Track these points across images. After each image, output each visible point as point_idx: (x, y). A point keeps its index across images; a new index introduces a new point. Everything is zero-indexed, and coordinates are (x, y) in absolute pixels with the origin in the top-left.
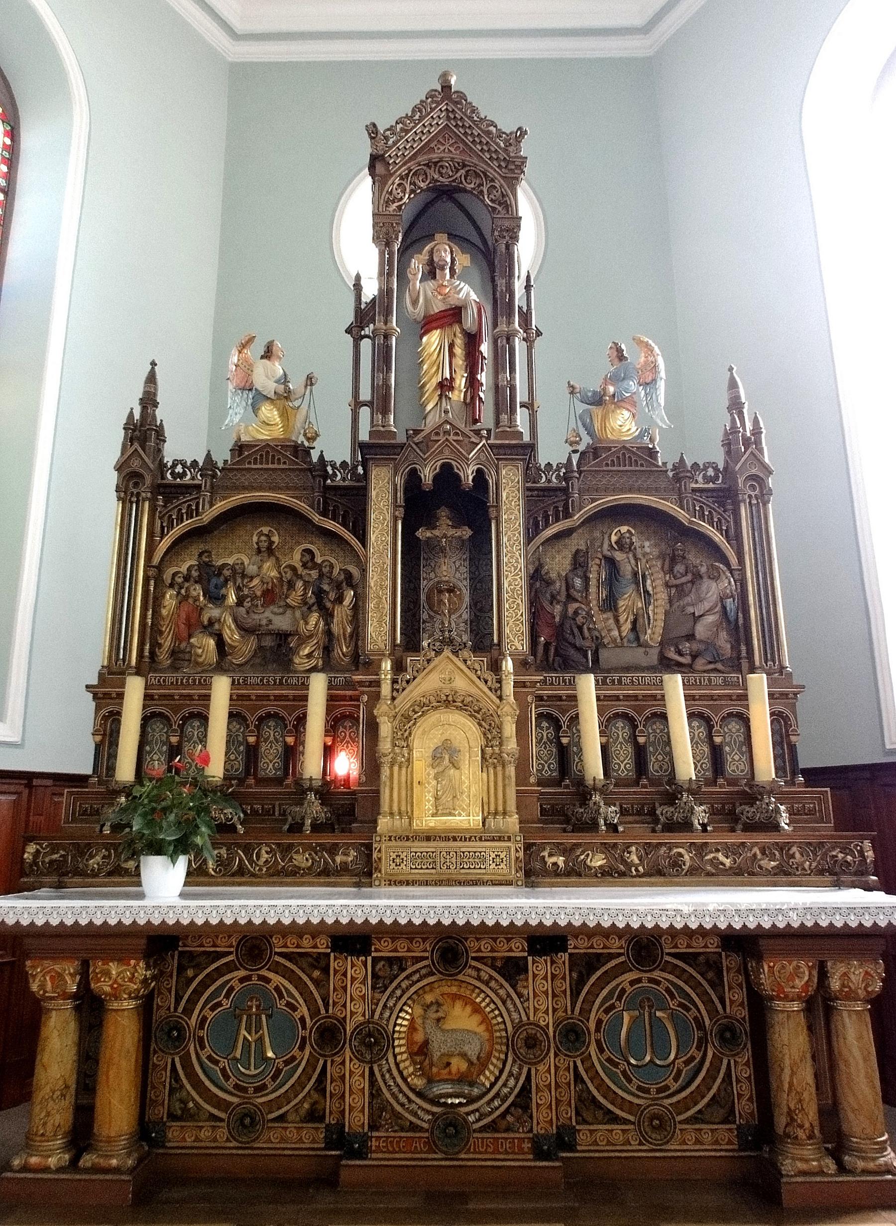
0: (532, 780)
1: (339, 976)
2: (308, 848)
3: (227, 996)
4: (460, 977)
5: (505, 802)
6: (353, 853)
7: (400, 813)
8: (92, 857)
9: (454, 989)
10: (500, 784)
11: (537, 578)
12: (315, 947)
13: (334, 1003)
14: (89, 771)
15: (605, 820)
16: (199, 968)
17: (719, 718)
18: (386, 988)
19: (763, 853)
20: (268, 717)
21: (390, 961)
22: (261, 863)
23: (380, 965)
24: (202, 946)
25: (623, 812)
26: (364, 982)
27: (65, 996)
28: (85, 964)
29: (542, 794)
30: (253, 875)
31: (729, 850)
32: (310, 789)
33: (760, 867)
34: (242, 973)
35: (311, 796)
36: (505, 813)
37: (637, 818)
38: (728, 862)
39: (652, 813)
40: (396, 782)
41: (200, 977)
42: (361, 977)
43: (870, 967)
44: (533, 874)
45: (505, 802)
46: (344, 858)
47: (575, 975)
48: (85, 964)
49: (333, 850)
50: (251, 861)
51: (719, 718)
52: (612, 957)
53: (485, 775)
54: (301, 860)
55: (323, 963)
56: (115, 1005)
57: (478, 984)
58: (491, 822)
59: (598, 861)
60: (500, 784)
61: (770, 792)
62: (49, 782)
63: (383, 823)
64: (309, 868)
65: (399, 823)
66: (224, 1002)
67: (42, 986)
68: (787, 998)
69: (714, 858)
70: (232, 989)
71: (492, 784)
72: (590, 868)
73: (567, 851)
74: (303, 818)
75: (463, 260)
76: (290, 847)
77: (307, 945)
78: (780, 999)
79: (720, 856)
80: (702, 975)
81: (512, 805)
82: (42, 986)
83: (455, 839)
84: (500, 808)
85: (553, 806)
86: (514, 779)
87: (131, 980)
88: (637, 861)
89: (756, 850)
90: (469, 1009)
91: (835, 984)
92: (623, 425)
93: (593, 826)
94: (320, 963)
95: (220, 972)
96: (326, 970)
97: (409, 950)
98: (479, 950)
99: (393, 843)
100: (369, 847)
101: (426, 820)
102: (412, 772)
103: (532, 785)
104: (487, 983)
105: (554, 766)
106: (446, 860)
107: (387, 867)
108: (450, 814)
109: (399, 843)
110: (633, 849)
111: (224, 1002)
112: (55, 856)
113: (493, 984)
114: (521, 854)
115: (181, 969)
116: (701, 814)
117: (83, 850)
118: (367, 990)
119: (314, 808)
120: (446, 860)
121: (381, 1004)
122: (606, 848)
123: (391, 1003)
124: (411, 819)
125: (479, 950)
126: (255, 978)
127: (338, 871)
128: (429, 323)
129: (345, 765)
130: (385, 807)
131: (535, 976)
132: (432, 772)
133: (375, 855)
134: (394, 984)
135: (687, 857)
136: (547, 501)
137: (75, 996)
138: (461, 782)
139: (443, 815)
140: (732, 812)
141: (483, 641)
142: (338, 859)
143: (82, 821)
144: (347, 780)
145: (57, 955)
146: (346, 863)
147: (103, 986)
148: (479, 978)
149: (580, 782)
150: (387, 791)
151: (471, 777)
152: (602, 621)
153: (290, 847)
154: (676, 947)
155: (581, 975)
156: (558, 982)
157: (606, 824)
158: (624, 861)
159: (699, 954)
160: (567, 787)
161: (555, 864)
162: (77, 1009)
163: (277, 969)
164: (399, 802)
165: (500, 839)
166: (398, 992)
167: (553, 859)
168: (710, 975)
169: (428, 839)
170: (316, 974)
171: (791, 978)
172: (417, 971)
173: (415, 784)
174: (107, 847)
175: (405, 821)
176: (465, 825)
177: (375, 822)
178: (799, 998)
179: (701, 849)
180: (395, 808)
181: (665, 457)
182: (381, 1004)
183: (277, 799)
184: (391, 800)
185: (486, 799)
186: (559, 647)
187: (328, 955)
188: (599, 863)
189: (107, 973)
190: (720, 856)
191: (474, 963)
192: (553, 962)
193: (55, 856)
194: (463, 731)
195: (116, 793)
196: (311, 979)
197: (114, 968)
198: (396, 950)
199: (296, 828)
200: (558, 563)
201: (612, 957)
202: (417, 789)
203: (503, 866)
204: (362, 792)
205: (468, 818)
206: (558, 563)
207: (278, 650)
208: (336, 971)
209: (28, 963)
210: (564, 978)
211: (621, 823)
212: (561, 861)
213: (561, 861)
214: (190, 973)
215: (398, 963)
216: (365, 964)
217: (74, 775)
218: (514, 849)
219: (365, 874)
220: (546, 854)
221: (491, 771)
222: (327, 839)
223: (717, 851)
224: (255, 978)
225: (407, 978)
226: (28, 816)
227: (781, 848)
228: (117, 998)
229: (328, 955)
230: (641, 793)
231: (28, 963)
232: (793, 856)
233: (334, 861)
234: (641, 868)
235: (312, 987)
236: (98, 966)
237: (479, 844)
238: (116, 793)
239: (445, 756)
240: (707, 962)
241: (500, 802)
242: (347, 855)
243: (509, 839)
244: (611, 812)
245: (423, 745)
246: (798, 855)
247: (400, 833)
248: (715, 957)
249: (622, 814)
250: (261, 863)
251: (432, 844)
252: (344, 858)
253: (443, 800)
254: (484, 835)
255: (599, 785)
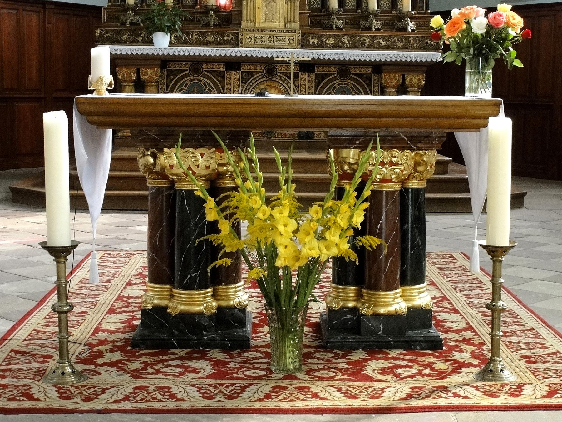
0: (307, 8)
1: (228, 80)
2: (212, 33)
3: (185, 86)
4: (274, 79)
5: (294, 17)
6: (231, 36)
7: (250, 20)
8: (123, 35)
9: (271, 84)
10: (293, 8)
12: (219, 68)
13: (227, 89)
15: (336, 25)
16: (175, 75)
18: (246, 82)
19: (398, 40)
21: (248, 73)
22: (193, 39)
23: (244, 74)
24: (176, 67)
25: (346, 23)
26: (238, 80)
27: (131, 81)
28: (138, 70)
29: (310, 14)
30: (191, 44)
31: (384, 38)
32: (212, 10)
33: (396, 45)
34: (191, 78)
35: (212, 13)
36: (294, 21)
37: (352, 26)
38: (383, 43)
39: (358, 24)
40: (249, 8)
41: (176, 79)
42: (237, 78)
43: (421, 77)
44: (304, 45)
45: (294, 17)
46: (228, 38)
47: (317, 81)
48: (138, 70)
49: (223, 34)
50: (189, 38)
52: (331, 74)
53: (286, 6)
54: (210, 38)
55: (222, 75)
56: (149, 84)
57: (280, 81)
58: (288, 25)
59: (331, 42)
60: (293, 8)
61: (407, 16)
62: (53, 6)
63: (244, 24)
64: (213, 42)
65: (250, 24)
66: (184, 88)
67: (123, 76)
68: (389, 87)
69: (379, 41)
70: (187, 84)
71: (289, 10)
72: (328, 44)
73: (319, 37)
74: (209, 22)
76: (205, 33)
77: (216, 68)
78: (388, 87)
79: (381, 41)
80: (364, 81)
81: (297, 18)
82: (123, 76)
83: (273, 31)
84: (292, 19)
85: (316, 20)
86: (298, 8)
87: (156, 75)
88: (347, 42)
89: (395, 38)
90: (277, 91)
91: (407, 82)
93: (331, 28)
94: (221, 75)
95: (183, 77)
96: (223, 77)
97: (255, 69)
98: (281, 70)
99: (248, 32)
100: (238, 34)
101: (261, 23)
102: (256, 3)
103: (306, 10)
104: (284, 82)
105: (319, 3)
107: (245, 41)
108: (271, 21)
109: (250, 32)
110: (346, 37)
111: (184, 88)
112: (109, 34)
113: (286, 82)
114: (300, 38)
115: (168, 76)
116: (377, 24)
117: (120, 33)
118: (240, 83)
119: (213, 18)
121: (244, 88)
122: (334, 36)
123: (248, 88)
124: (255, 23)
125: (281, 70)
126: (196, 80)
127: (224, 43)
130: (244, 17)
131: (301, 79)
132: (264, 4)
133: (240, 37)
134: (249, 81)
135: (367, 41)
137: (134, 82)
138: (276, 8)
139: (268, 22)
140: (392, 25)
142: (225, 38)
143: (111, 22)
144: (225, 7)
145: (127, 66)
146: (228, 40)
147: (145, 77)
148: (281, 80)
149: (328, 10)
150: (245, 11)
153: (205, 33)
154: (355, 71)
155: (319, 80)
156: (310, 83)
157: (336, 27)
158: (341, 42)
159: (364, 74)
160: (324, 12)
161: (313, 42)
162: (134, 86)
163: (204, 76)
164: (250, 16)
165: (292, 32)
166: (251, 84)
167: (313, 40)
168: (367, 82)
169: (262, 31)
170: (219, 78)
171: (392, 79)
172: (258, 77)
173: (257, 8)
174: (130, 31)
175: (252, 24)
176: (277, 26)
177: (240, 24)
178: (394, 87)
179: (373, 38)
180: (248, 18)
182: (244, 88)
183: (196, 14)
184: (247, 15)
185: (286, 16)
187: (224, 72)
188: (332, 42)
189: (147, 73)
190: (381, 41)
191: (279, 74)
192: (309, 76)
193: (109, 34)
195: (128, 9)
196: (218, 80)
197: (149, 72)
198: (250, 69)
199: (207, 25)
201: (331, 74)
202: (257, 10)
203: (292, 42)
204: (234, 11)
205: (279, 23)
208: (227, 78)
209: (117, 69)
210: (313, 82)
211: (344, 28)
212: (316, 41)
213: (316, 41)
214: (172, 77)
215: (251, 74)
216: (239, 73)
217: (61, 2)
218: (297, 36)
219: (237, 43)
220: (310, 38)
221: (289, 3)
222: (221, 30)
223: (380, 39)
224: (196, 80)
225: (254, 79)
226: (45, 25)
227: (406, 38)
228: (150, 81)
229: (224, 72)
230: (356, 15)
231: (117, 69)
232: (410, 41)
233: (223, 39)
234: (348, 45)
235: (218, 83)
236: (143, 70)
237: (283, 33)
238: (128, 9)
240: (367, 77)
241: (292, 16)
242: (229, 36)
243: (295, 32)
244: (341, 23)
246: (412, 41)
247: (250, 28)
248: (369, 76)
249: (346, 24)
250: (193, 39)
251: (264, 33)
252: (228, 38)
253: (269, 15)
254: (285, 30)
255: (335, 11)
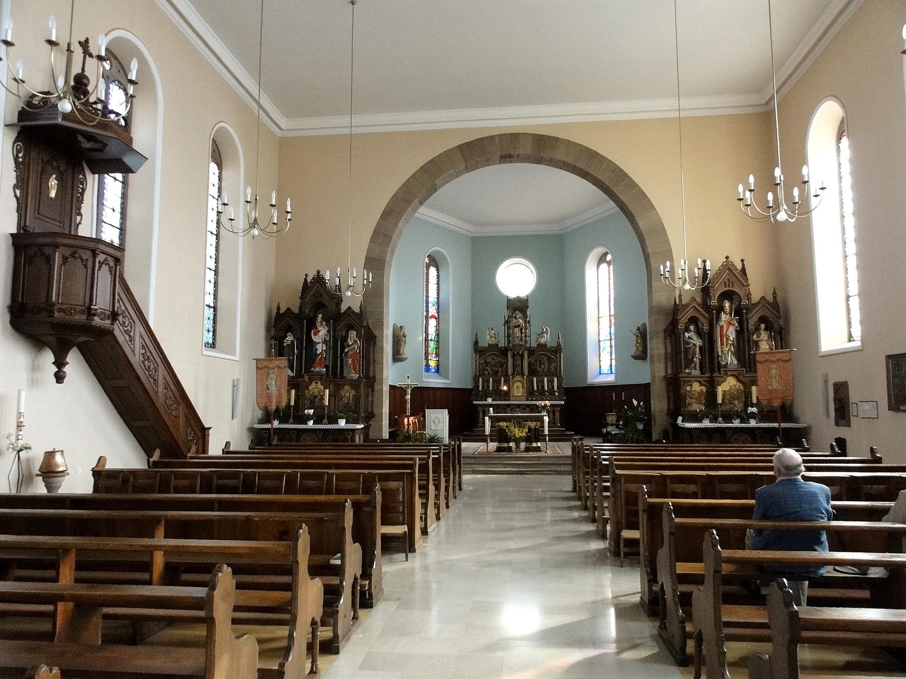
11: (529, 363)
14: (571, 477)
17: (551, 382)
20: (497, 383)
44: (527, 400)
51: (551, 382)
75: (520, 315)
92: (542, 341)
106: (516, 399)
120: (516, 399)
128: (516, 327)
129: (505, 388)
136: (531, 352)
141: (523, 374)
151: (521, 389)
152: (539, 369)
181: (548, 345)
186: (533, 372)
194: (520, 384)
200: (533, 361)
206: (533, 361)
207: (496, 373)
239: (518, 387)
245: (515, 386)
